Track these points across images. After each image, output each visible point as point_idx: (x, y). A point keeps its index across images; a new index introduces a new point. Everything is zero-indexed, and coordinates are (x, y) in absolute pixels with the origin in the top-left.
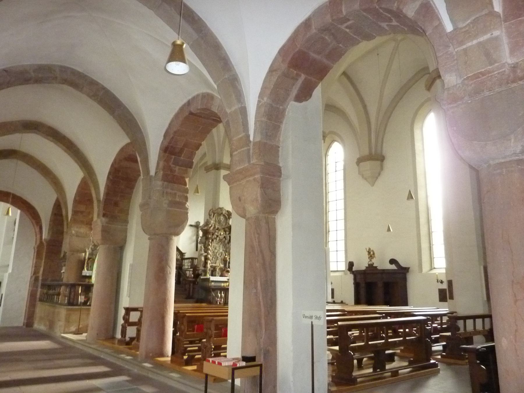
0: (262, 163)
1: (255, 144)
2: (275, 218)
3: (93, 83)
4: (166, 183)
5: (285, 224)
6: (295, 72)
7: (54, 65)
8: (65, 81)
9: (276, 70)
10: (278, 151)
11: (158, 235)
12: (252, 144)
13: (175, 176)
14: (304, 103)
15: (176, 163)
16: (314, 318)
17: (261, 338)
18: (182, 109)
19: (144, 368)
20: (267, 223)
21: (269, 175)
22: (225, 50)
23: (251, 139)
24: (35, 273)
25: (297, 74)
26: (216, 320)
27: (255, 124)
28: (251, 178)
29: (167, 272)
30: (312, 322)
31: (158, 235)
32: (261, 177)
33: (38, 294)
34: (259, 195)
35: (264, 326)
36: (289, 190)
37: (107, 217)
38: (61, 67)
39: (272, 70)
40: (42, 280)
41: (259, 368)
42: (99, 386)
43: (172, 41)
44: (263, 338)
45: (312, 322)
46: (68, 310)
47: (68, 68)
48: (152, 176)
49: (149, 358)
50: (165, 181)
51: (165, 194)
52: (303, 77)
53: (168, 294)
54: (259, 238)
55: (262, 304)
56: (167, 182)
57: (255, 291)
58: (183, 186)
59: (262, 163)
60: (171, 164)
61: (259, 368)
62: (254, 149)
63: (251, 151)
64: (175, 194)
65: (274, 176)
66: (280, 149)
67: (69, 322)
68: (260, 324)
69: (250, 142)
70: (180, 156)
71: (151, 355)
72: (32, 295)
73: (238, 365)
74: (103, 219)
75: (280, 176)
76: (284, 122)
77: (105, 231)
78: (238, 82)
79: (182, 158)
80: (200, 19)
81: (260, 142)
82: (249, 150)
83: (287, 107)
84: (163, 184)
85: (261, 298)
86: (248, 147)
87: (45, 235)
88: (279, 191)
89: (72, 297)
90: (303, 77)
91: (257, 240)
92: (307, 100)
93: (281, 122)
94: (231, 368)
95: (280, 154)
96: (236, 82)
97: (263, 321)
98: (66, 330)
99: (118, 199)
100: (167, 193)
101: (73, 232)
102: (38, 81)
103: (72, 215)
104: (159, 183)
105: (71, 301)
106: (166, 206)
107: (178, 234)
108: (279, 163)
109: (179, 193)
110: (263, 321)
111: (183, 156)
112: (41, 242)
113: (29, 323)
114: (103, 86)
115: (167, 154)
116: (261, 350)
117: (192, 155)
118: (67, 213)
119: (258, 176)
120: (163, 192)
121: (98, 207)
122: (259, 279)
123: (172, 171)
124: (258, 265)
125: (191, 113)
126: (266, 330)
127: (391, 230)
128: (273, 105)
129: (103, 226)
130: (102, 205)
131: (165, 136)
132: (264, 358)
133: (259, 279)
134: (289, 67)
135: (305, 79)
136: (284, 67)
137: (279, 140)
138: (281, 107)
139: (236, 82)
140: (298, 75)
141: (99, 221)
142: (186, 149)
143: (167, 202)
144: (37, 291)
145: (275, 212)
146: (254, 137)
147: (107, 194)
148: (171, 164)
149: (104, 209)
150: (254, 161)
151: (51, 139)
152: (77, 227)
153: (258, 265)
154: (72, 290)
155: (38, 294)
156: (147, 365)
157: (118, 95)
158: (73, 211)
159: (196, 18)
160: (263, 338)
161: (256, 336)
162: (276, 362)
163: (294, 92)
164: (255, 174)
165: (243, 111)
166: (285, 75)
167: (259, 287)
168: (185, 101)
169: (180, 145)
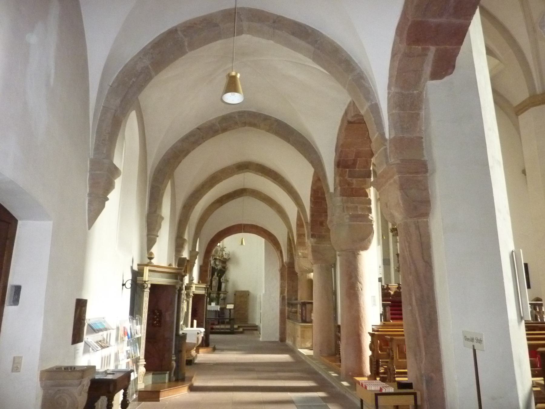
0: (399, 162)
1: (391, 140)
2: (427, 221)
3: (266, 118)
4: (345, 198)
5: (439, 226)
6: (420, 47)
7: (233, 113)
8: (245, 124)
9: (396, 54)
10: (422, 142)
11: (344, 251)
12: (388, 142)
13: (353, 188)
14: (446, 79)
15: (352, 176)
16: (475, 341)
17: (422, 362)
18: (343, 120)
19: (342, 385)
20: (418, 228)
21: (410, 173)
22: (345, 52)
23: (387, 136)
24: (282, 293)
25: (424, 49)
26: (397, 340)
27: (389, 119)
28: (392, 181)
29: (358, 288)
30: (473, 346)
31: (344, 251)
32: (399, 177)
33: (286, 311)
34: (399, 198)
35: (423, 348)
36: (442, 186)
37: (315, 237)
38: (239, 112)
39: (394, 55)
40: (288, 299)
41: (379, 397)
42: (294, 399)
43: (228, 73)
44: (423, 363)
45: (473, 346)
46: (302, 327)
47: (245, 111)
48: (331, 193)
49: (350, 377)
50: (343, 196)
51: (345, 208)
52: (433, 49)
53: (362, 311)
54: (409, 247)
55: (419, 323)
56: (346, 196)
57: (410, 308)
58: (364, 198)
59: (399, 162)
60: (347, 177)
61: (379, 397)
62: (390, 147)
63: (388, 151)
64: (357, 207)
65: (417, 173)
66: (423, 140)
67: (304, 338)
68: (419, 346)
69: (386, 140)
70: (355, 168)
71: (350, 373)
72: (282, 313)
73: (384, 391)
74: (312, 240)
75: (426, 171)
76: (424, 108)
77: (315, 251)
78: (364, 80)
79: (357, 169)
80: (313, 30)
81: (394, 138)
82: (386, 149)
83: (424, 89)
84: (342, 200)
85: (417, 315)
86: (385, 147)
87: (285, 259)
88: (426, 189)
89: (304, 314)
90: (433, 49)
91: (408, 249)
92: (451, 73)
93: (420, 109)
94: (373, 393)
95: (424, 145)
96: (362, 81)
97: (422, 344)
98: (303, 345)
99: (323, 219)
100: (347, 207)
101: (300, 254)
102: (224, 130)
103: (298, 238)
104: (339, 199)
105: (304, 318)
106: (347, 221)
107: (365, 248)
108: (423, 156)
109: (359, 206)
110: (422, 344)
111: (357, 167)
112: (283, 265)
113: (283, 339)
114: (276, 119)
115: (341, 169)
116: (422, 376)
117: (368, 163)
118: (293, 239)
119: (396, 177)
120: (343, 207)
121: (307, 228)
122: (413, 294)
123: (349, 184)
124: (411, 277)
125: (350, 122)
126: (426, 353)
127: (244, 244)
128: (403, 92)
129: (312, 246)
130: (309, 227)
131: (336, 151)
132: (427, 386)
133: (413, 294)
134: (409, 44)
135: (437, 50)
136: (403, 47)
137: (421, 129)
138: (415, 92)
139: (362, 81)
140: (425, 50)
141: (309, 242)
142: (359, 159)
143: (348, 216)
144: (285, 309)
145: (426, 214)
146: (390, 134)
147: (312, 215)
148: (347, 177)
149: (311, 231)
150: (392, 160)
151: (260, 174)
152: (303, 249)
153: (411, 277)
154: (303, 308)
155: (286, 311)
156: (345, 384)
157: (289, 123)
158: (297, 234)
159: (310, 31)
160: (423, 363)
161: (416, 360)
162: (443, 393)
163: (428, 69)
164: (392, 177)
165: (375, 109)
166: (408, 55)
167: (414, 303)
168: (343, 113)
169: (352, 157)
